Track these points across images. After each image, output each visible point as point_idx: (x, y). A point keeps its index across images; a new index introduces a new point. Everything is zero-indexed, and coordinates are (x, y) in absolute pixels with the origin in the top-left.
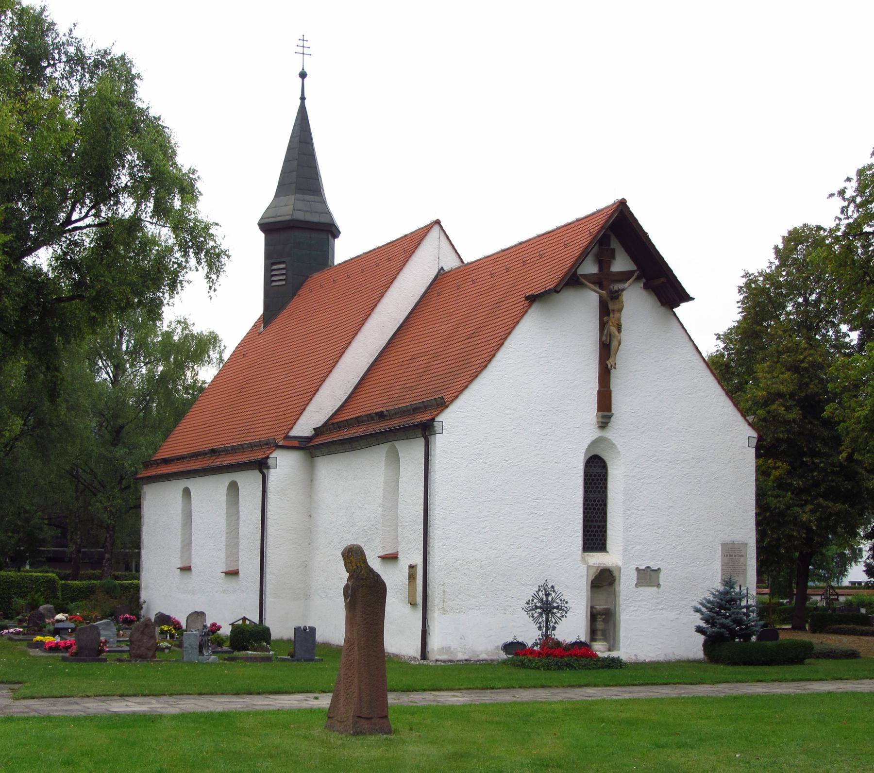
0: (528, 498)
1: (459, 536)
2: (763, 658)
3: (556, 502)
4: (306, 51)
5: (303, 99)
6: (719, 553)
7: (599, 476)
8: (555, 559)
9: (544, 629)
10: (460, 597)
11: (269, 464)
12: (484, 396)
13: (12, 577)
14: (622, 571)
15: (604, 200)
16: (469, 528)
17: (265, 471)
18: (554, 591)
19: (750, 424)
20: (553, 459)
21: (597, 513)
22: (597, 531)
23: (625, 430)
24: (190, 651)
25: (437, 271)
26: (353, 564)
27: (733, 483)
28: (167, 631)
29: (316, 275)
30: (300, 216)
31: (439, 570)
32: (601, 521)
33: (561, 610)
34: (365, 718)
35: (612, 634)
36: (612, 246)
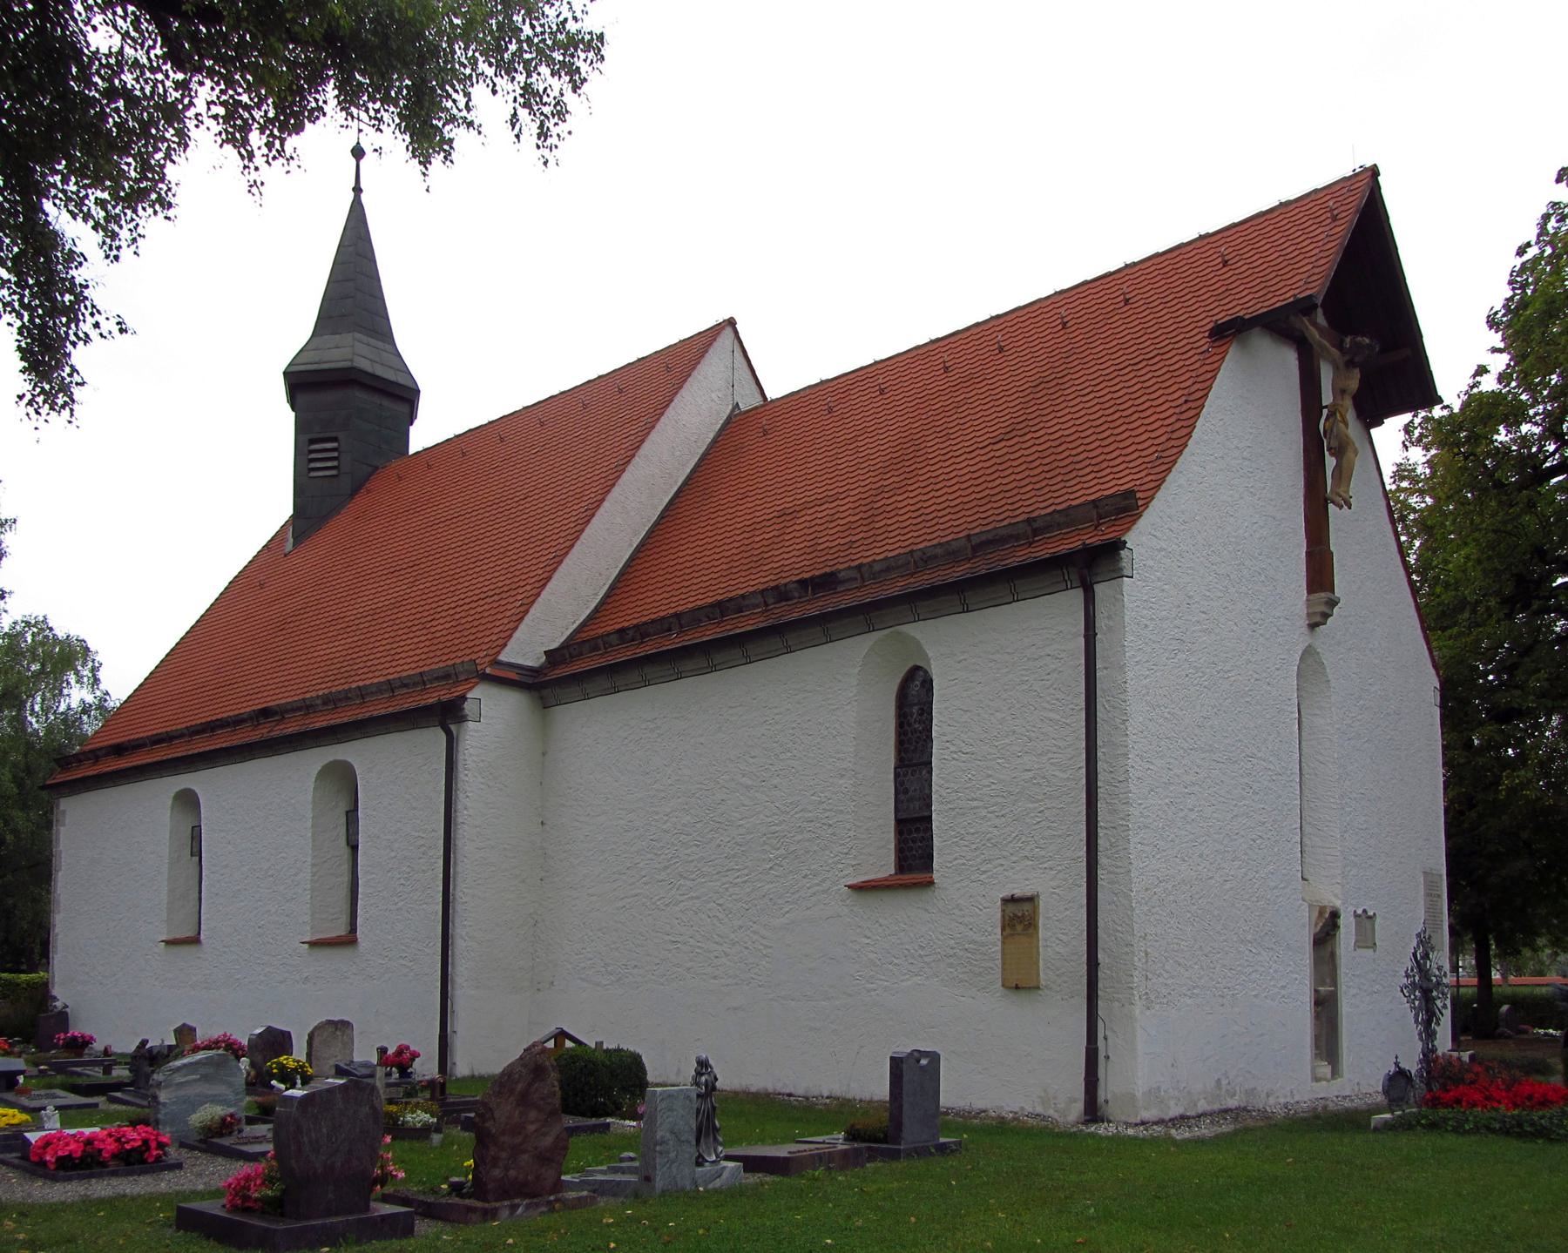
5: (357, 190)
11: (467, 712)
15: (1343, 168)
17: (453, 728)
24: (672, 1155)
28: (295, 1069)
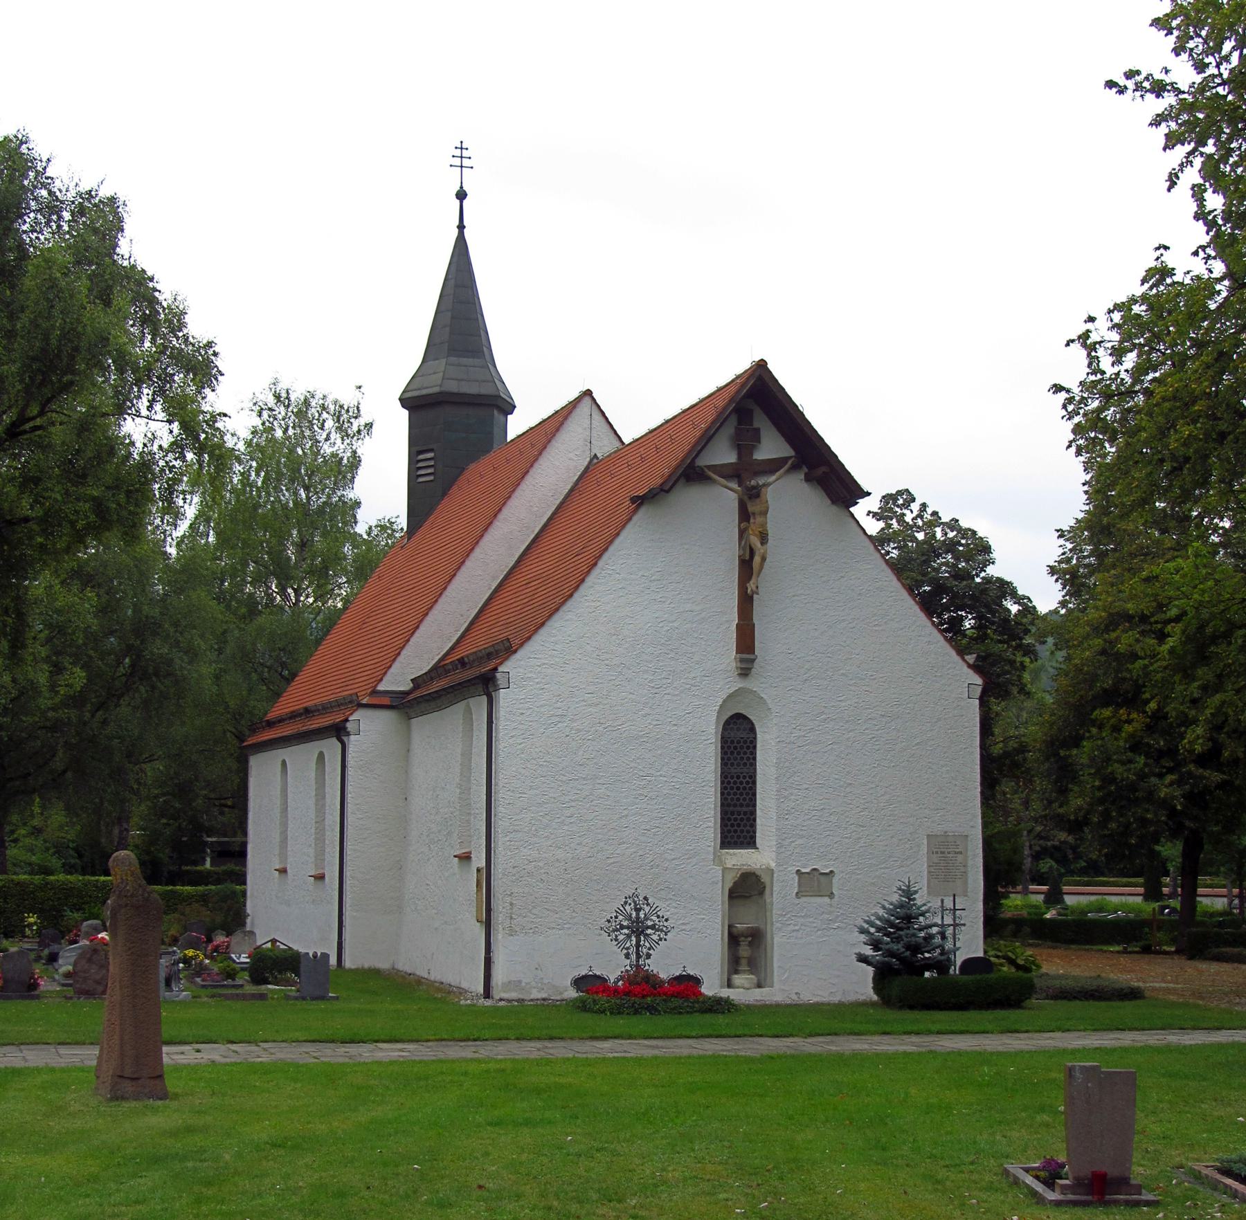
0: (633, 775)
1: (533, 829)
2: (952, 1000)
3: (676, 780)
4: (466, 162)
5: (461, 227)
6: (924, 849)
7: (745, 742)
8: (673, 859)
9: (634, 957)
10: (534, 911)
12: (569, 636)
13: (71, 882)
14: (775, 875)
15: (742, 365)
16: (548, 818)
17: (345, 739)
18: (648, 904)
19: (969, 666)
20: (670, 720)
21: (741, 794)
22: (742, 820)
23: (778, 678)
25: (588, 459)
26: (118, 877)
27: (945, 750)
29: (472, 466)
30: (453, 387)
31: (504, 874)
32: (748, 806)
33: (657, 930)
34: (128, 1078)
35: (763, 963)
36: (756, 425)
